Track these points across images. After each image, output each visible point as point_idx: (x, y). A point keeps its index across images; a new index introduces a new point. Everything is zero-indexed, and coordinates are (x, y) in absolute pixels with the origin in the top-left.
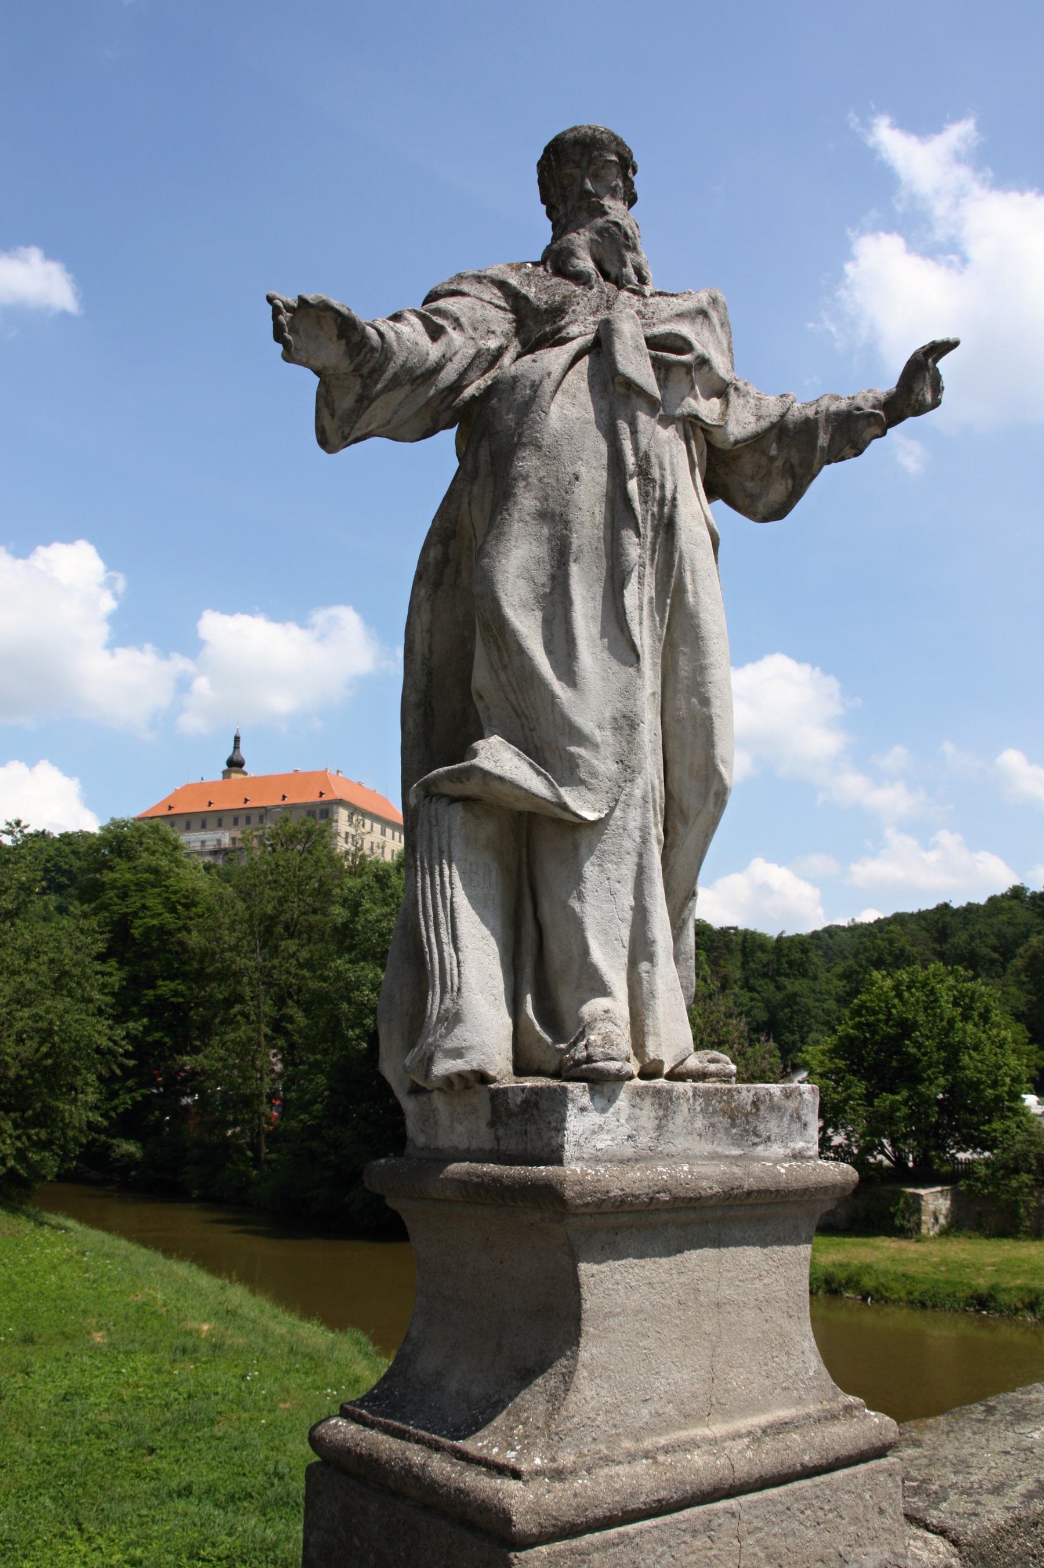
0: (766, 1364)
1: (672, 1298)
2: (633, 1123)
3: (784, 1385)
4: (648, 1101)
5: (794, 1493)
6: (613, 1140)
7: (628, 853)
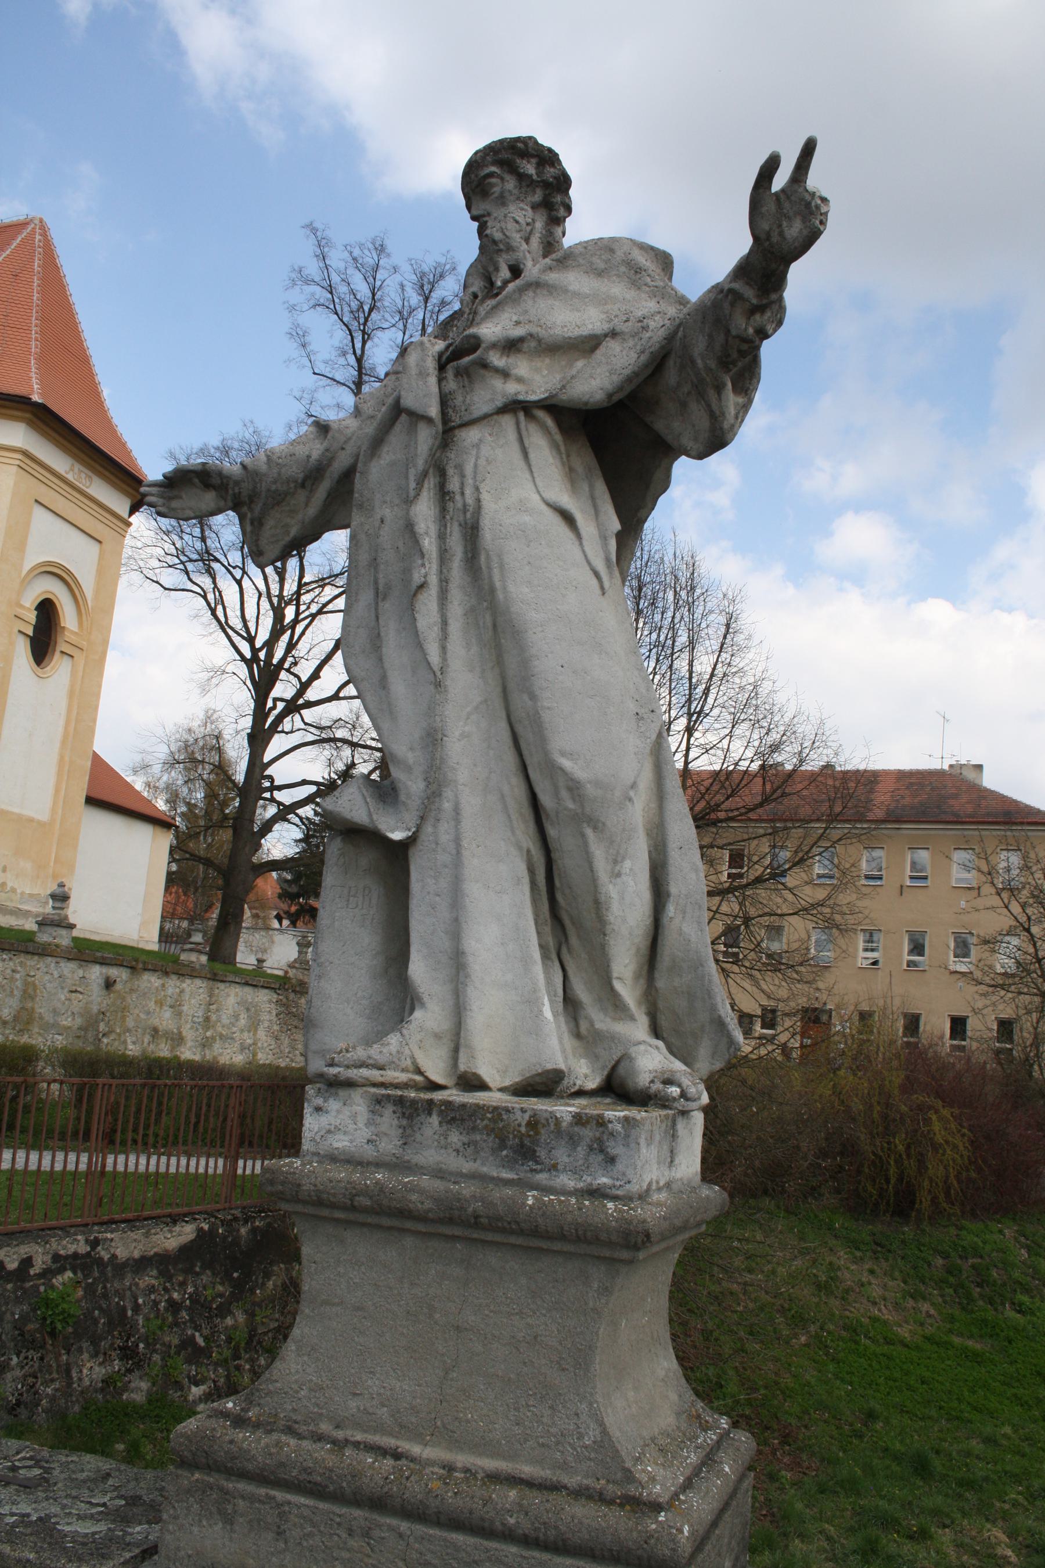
0: (517, 1409)
1: (399, 1305)
2: (373, 1128)
3: (541, 1440)
4: (388, 1111)
5: (487, 1551)
6: (351, 1141)
7: (446, 866)
